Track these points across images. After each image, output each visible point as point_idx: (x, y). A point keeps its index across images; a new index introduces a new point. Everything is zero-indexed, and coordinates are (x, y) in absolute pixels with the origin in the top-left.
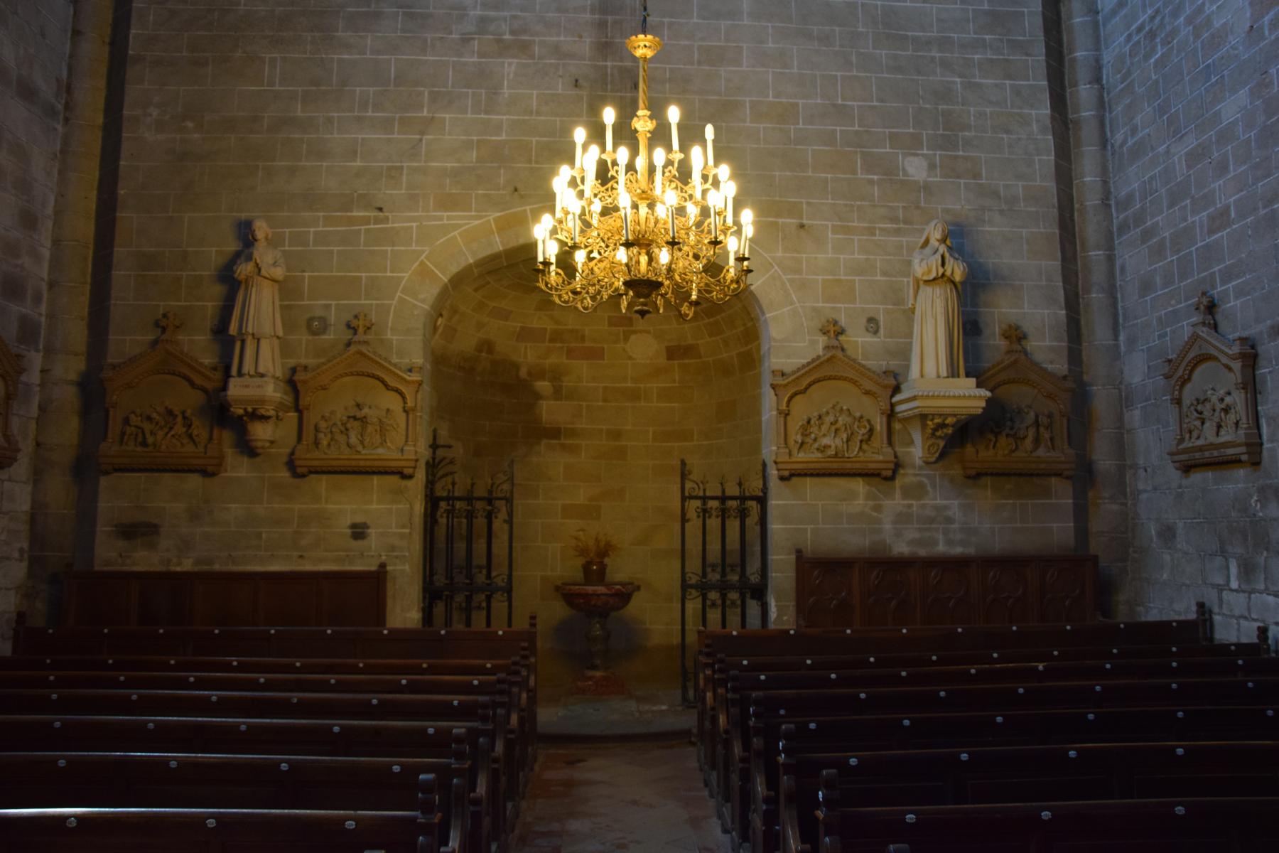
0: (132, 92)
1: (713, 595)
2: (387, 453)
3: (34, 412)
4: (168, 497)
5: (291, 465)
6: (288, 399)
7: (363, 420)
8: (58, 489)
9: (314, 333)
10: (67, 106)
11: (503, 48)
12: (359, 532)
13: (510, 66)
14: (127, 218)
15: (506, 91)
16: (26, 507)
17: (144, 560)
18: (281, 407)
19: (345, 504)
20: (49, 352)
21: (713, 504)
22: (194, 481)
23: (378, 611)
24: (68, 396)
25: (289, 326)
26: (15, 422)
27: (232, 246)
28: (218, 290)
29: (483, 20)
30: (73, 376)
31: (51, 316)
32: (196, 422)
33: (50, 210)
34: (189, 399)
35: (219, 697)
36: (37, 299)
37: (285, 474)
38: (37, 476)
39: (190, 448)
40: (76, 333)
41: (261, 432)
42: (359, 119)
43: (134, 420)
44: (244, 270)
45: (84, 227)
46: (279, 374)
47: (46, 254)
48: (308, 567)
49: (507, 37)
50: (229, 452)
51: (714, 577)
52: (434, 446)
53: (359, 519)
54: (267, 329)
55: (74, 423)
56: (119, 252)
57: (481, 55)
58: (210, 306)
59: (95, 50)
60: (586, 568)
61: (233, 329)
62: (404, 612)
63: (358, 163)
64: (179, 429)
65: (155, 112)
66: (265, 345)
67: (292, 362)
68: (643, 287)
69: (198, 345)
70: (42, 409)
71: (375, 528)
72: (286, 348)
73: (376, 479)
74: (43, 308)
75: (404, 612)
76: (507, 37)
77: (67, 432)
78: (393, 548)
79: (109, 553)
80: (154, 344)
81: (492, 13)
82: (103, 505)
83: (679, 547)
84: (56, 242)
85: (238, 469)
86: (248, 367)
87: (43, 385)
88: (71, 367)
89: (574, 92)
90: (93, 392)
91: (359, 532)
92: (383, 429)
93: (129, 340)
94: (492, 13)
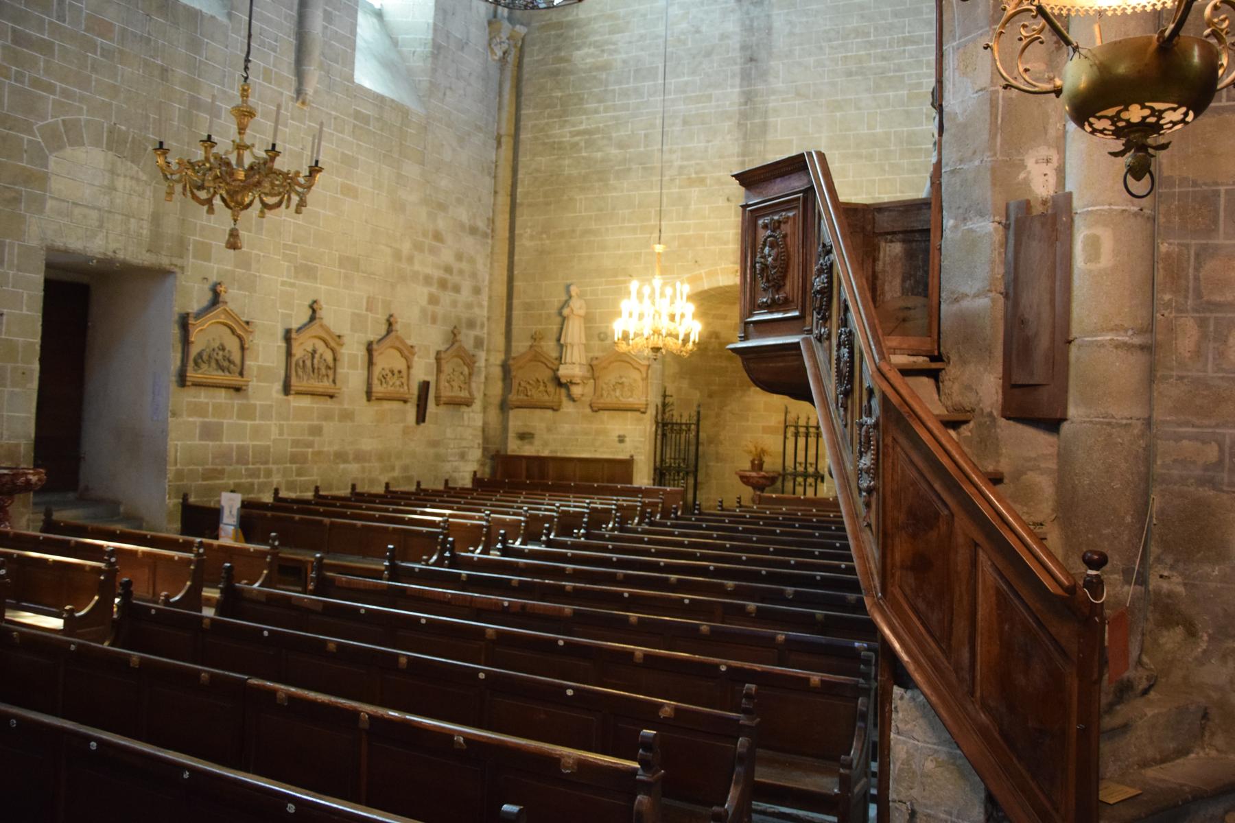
0: (519, 222)
1: (800, 479)
2: (636, 399)
3: (482, 379)
4: (537, 421)
5: (591, 406)
6: (588, 375)
7: (622, 384)
8: (494, 415)
9: (602, 340)
10: (493, 231)
11: (691, 182)
12: (621, 439)
13: (695, 192)
14: (519, 284)
15: (693, 207)
16: (480, 423)
17: (528, 450)
18: (583, 378)
19: (616, 425)
20: (488, 351)
21: (802, 430)
22: (549, 413)
23: (629, 478)
24: (497, 372)
25: (589, 336)
26: (474, 385)
27: (564, 298)
28: (559, 319)
29: (681, 167)
30: (499, 362)
31: (489, 334)
32: (549, 384)
33: (486, 283)
34: (548, 374)
35: (631, 594)
36: (482, 326)
37: (588, 410)
38: (485, 409)
39: (546, 398)
40: (500, 341)
41: (576, 391)
42: (621, 228)
43: (523, 384)
44: (566, 312)
45: (502, 290)
46: (584, 361)
47: (485, 303)
48: (598, 456)
49: (693, 176)
50: (564, 399)
51: (800, 469)
52: (665, 396)
53: (621, 433)
54: (576, 340)
55: (500, 384)
56: (516, 302)
57: (680, 187)
58: (555, 328)
59: (503, 199)
60: (753, 462)
61: (562, 341)
62: (643, 478)
63: (621, 252)
64: (542, 388)
65: (529, 230)
66: (576, 348)
67: (591, 355)
68: (656, 349)
69: (549, 347)
70: (486, 378)
71: (630, 439)
72: (587, 348)
73: (629, 414)
74: (485, 330)
75: (643, 478)
76: (693, 176)
77: (497, 389)
78: (637, 448)
79: (514, 447)
80: (531, 346)
81: (685, 163)
82: (511, 424)
83: (781, 450)
84: (490, 298)
85: (568, 407)
86: (568, 360)
87: (486, 367)
88: (497, 358)
89: (727, 204)
90: (506, 369)
91: (621, 439)
92: (632, 391)
93: (521, 346)
94: (685, 163)
